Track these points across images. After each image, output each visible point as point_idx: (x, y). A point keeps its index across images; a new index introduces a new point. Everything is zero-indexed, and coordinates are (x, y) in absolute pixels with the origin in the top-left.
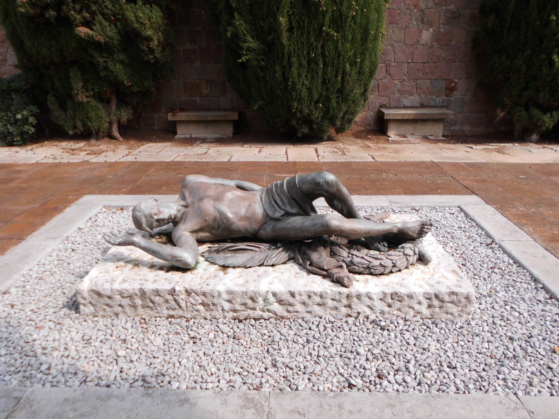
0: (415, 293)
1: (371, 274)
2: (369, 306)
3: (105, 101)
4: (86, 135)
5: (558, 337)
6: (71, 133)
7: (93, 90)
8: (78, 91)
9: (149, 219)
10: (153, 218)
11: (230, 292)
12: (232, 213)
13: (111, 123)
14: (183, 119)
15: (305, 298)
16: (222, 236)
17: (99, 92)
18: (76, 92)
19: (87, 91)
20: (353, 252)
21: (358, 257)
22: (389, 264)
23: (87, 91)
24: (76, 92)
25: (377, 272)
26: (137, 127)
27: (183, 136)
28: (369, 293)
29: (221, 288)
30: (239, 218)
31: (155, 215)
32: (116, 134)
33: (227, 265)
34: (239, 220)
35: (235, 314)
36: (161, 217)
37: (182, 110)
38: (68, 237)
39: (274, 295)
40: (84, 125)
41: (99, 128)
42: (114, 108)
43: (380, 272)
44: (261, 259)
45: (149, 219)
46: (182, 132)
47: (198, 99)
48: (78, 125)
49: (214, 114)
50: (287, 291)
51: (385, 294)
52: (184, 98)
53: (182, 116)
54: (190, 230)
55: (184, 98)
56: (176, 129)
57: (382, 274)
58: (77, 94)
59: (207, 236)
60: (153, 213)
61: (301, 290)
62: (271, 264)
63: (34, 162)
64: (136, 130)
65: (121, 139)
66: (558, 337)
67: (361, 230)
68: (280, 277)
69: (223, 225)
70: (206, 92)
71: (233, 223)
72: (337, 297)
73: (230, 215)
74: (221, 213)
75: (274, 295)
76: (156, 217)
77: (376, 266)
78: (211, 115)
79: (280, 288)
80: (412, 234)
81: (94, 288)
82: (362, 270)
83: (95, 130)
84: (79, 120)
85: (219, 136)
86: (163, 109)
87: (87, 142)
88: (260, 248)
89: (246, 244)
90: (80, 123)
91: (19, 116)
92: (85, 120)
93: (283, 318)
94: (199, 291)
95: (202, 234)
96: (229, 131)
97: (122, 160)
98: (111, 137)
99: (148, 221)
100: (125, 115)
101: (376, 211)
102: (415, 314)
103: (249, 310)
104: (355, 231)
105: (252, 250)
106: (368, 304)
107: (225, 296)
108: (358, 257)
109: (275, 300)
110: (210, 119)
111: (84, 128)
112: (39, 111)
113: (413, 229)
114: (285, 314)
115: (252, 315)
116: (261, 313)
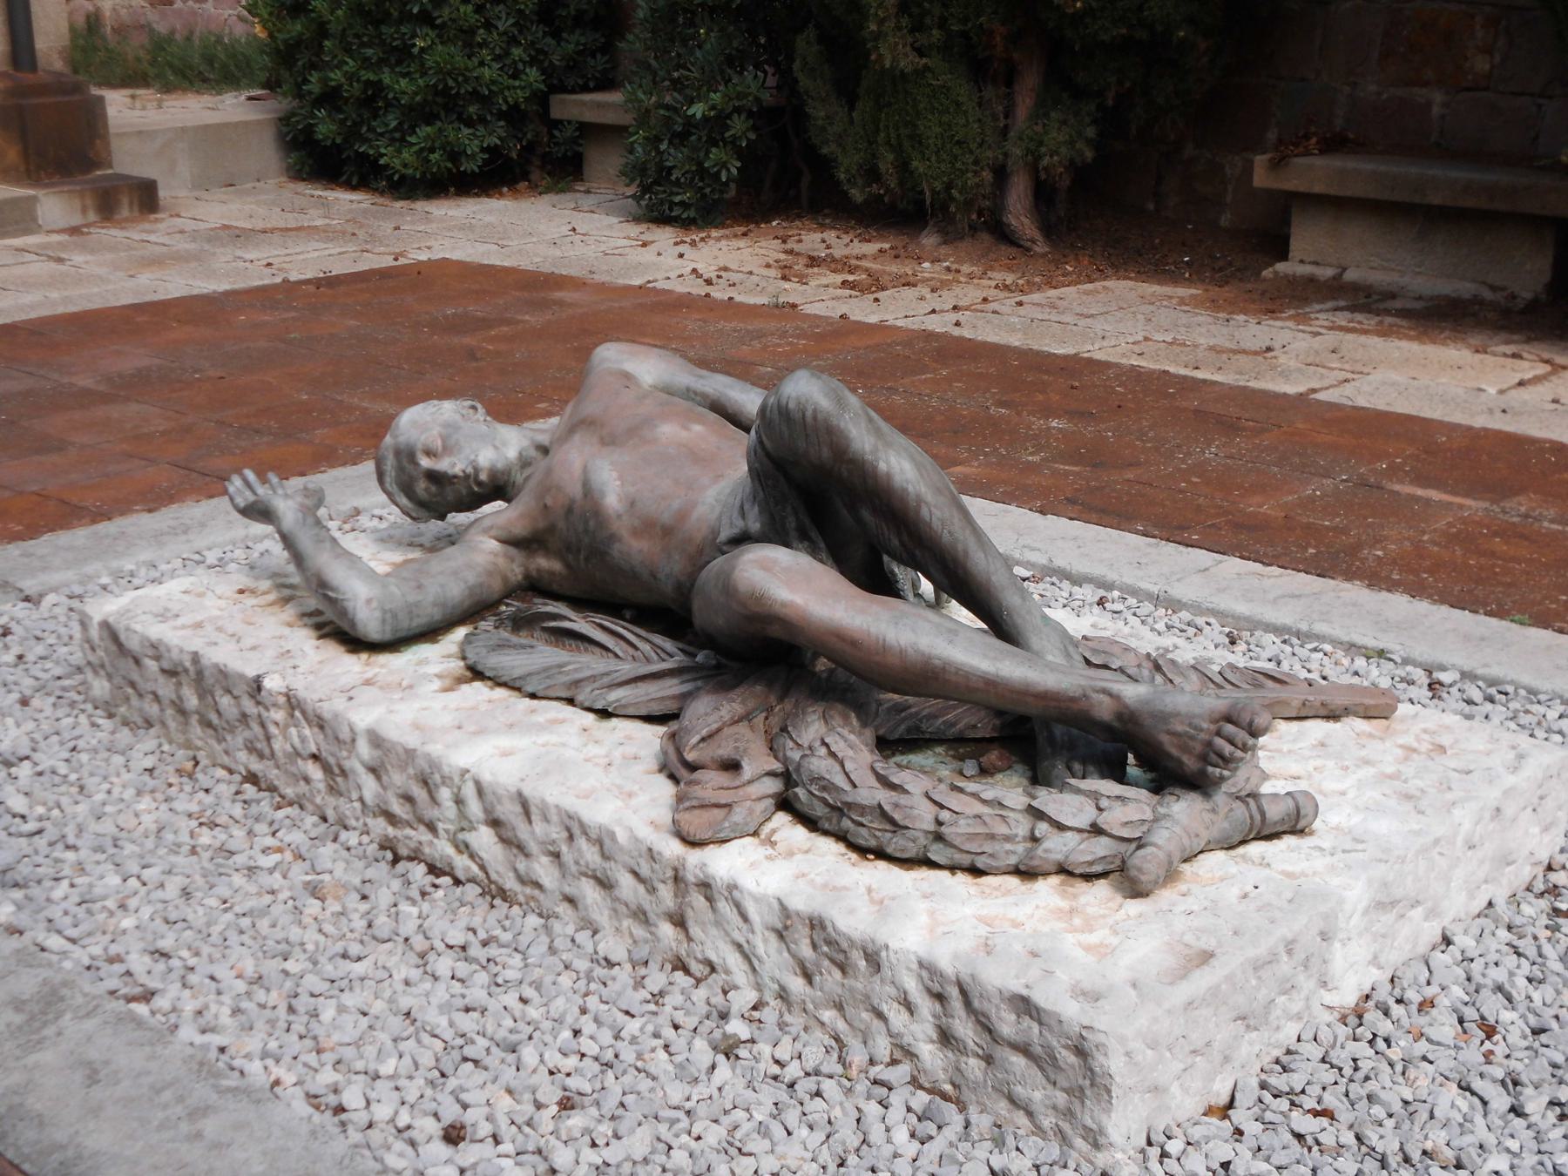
0: (887, 947)
1: (841, 837)
3: (987, 70)
4: (902, 212)
6: (857, 195)
7: (942, 24)
8: (881, 22)
10: (417, 464)
11: (376, 740)
13: (1001, 174)
14: (1318, 188)
15: (557, 833)
17: (964, 35)
18: (873, 27)
19: (918, 27)
20: (1047, 799)
22: (923, 816)
23: (918, 27)
24: (873, 27)
25: (864, 838)
26: (1151, 206)
27: (1307, 269)
30: (636, 523)
31: (429, 453)
32: (1019, 213)
33: (480, 668)
34: (635, 533)
35: (391, 831)
37: (1334, 144)
38: (357, 512)
40: (903, 167)
41: (949, 186)
42: (1024, 105)
43: (873, 843)
45: (405, 464)
46: (1312, 250)
47: (1438, 97)
48: (882, 167)
49: (1460, 174)
50: (513, 790)
52: (1373, 88)
53: (1314, 172)
54: (504, 535)
55: (1373, 88)
56: (1289, 225)
57: (881, 854)
58: (877, 36)
59: (552, 573)
60: (419, 446)
61: (550, 800)
62: (599, 706)
63: (637, 282)
64: (1104, 214)
65: (1041, 248)
67: (885, 649)
68: (577, 759)
69: (586, 540)
70: (1482, 64)
71: (613, 538)
74: (587, 489)
76: (425, 462)
78: (1443, 181)
80: (1174, 751)
81: (111, 620)
82: (819, 811)
83: (933, 191)
84: (888, 143)
85: (1463, 288)
86: (1272, 136)
87: (900, 241)
90: (891, 157)
91: (698, 110)
92: (906, 144)
93: (503, 894)
94: (309, 709)
95: (545, 563)
96: (1527, 272)
97: (900, 323)
98: (1003, 235)
100: (1065, 141)
101: (1100, 599)
102: (898, 1055)
103: (422, 828)
104: (854, 643)
107: (364, 749)
110: (1436, 199)
111: (901, 184)
113: (1180, 728)
114: (510, 883)
115: (427, 850)
116: (450, 850)
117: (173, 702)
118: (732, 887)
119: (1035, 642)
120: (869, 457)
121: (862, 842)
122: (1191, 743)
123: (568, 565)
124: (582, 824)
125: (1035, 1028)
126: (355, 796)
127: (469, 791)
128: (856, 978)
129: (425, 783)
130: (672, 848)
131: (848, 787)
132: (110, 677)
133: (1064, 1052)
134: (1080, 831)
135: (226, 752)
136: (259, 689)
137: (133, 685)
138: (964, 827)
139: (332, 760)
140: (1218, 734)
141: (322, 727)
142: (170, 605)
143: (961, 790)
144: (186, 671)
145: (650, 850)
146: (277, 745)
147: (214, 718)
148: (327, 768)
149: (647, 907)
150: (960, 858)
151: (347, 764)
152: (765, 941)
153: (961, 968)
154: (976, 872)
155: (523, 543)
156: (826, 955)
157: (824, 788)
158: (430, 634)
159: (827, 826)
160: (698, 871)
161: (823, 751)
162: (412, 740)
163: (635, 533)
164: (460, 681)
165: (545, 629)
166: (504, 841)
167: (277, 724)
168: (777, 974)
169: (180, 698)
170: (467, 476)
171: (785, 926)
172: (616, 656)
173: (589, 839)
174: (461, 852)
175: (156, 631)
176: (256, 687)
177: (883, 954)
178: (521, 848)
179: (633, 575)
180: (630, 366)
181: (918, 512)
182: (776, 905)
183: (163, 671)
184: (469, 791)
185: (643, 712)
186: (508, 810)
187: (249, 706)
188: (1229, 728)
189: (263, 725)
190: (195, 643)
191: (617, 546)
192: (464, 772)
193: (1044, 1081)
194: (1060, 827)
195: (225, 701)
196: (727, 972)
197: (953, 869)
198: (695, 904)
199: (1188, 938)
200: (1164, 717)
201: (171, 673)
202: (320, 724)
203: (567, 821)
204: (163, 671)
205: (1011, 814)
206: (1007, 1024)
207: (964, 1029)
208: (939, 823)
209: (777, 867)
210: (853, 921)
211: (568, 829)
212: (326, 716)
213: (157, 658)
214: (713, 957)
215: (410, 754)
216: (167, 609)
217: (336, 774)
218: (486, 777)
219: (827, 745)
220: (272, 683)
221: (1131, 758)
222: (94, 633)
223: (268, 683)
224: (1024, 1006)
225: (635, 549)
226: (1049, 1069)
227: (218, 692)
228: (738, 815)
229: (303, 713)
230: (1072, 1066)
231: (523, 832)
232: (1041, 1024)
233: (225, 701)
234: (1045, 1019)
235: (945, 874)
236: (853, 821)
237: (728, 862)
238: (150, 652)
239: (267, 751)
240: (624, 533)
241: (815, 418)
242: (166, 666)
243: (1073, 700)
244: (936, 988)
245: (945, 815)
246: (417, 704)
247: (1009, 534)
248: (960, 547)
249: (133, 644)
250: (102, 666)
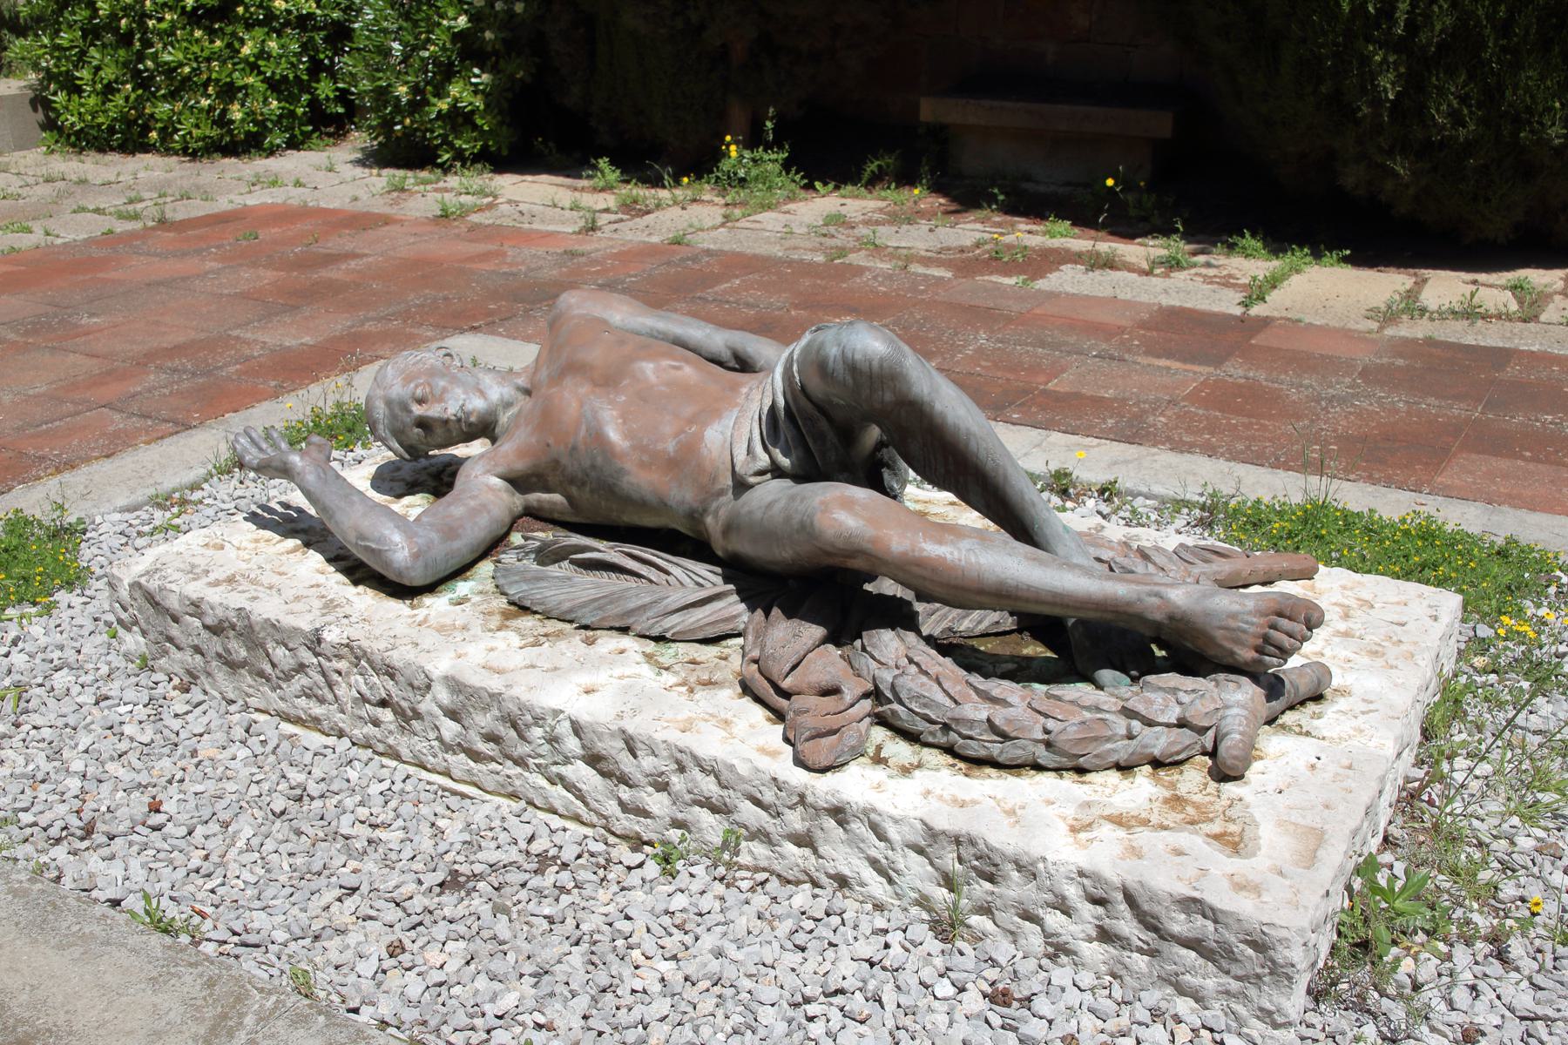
0: (1044, 859)
1: (949, 750)
2: (874, 863)
5: (3, 754)
9: (397, 410)
11: (455, 685)
12: (628, 435)
15: (665, 765)
16: (594, 514)
21: (926, 673)
25: (975, 750)
28: (874, 810)
29: (440, 666)
31: (420, 401)
33: (527, 603)
36: (433, 411)
39: (577, 729)
43: (982, 753)
44: (1365, 798)
45: (397, 410)
51: (933, 834)
59: (555, 503)
62: (655, 632)
66: (3, 754)
68: (656, 689)
72: (768, 796)
73: (614, 435)
75: (577, 729)
76: (418, 410)
77: (971, 723)
79: (598, 711)
88: (667, 573)
89: (628, 548)
94: (377, 658)
99: (394, 416)
101: (1123, 515)
103: (509, 763)
105: (639, 576)
106: (873, 853)
107: (443, 695)
108: (926, 673)
109: (579, 751)
112: (924, 160)
117: (219, 656)
118: (274, 626)
119: (1061, 550)
120: (926, 399)
121: (971, 753)
122: (1244, 636)
123: (569, 497)
124: (695, 757)
125: (1210, 926)
126: (432, 735)
127: (564, 728)
128: (1009, 887)
129: (514, 726)
130: (799, 778)
131: (948, 702)
132: (144, 633)
133: (1242, 946)
134: (1168, 725)
135: (282, 699)
136: (319, 641)
137: (170, 639)
138: (1073, 732)
139: (404, 704)
140: (1273, 627)
141: (392, 676)
142: (196, 561)
143: (1058, 698)
144: (233, 627)
145: (775, 779)
146: (342, 691)
147: (268, 668)
148: (399, 712)
149: (771, 829)
150: (1065, 761)
151: (422, 708)
152: (905, 856)
153: (1125, 876)
154: (1081, 771)
155: (518, 482)
156: (974, 868)
157: (925, 706)
158: (461, 571)
159: (931, 739)
160: (829, 797)
161: (913, 669)
162: (494, 684)
163: (642, 465)
164: (507, 616)
165: (573, 562)
166: (603, 774)
167: (339, 673)
168: (919, 884)
169: (228, 651)
170: (459, 420)
171: (929, 841)
172: (651, 581)
173: (703, 770)
174: (553, 784)
175: (194, 590)
176: (315, 642)
177: (1041, 866)
178: (624, 780)
179: (643, 505)
180: (606, 315)
181: (967, 445)
182: (919, 825)
183: (206, 627)
184: (564, 728)
185: (700, 636)
186: (612, 746)
187: (307, 657)
188: (1284, 623)
189: (324, 674)
190: (236, 600)
191: (626, 479)
192: (556, 713)
193: (1215, 970)
194: (1150, 723)
195: (280, 653)
196: (863, 885)
197: (1057, 770)
198: (825, 825)
199: (1295, 817)
200: (1207, 614)
201: (216, 630)
202: (390, 672)
203: (679, 755)
204: (206, 627)
205: (1107, 716)
206: (1178, 924)
207: (1127, 926)
208: (1047, 732)
209: (908, 791)
210: (1001, 837)
211: (678, 762)
212: (397, 664)
213: (199, 615)
214: (846, 871)
215: (496, 697)
216: (193, 566)
217: (408, 717)
218: (584, 718)
219: (918, 665)
220: (332, 636)
221: (1154, 647)
222: (124, 593)
223: (325, 635)
224: (1192, 905)
225: (641, 479)
226: (1224, 963)
227: (270, 646)
228: (850, 737)
229: (369, 662)
230: (1250, 958)
231: (626, 763)
232: (1216, 922)
233: (280, 653)
234: (1221, 917)
235: (1052, 774)
236: (960, 734)
237: (853, 784)
238: (191, 609)
239: (330, 697)
240: (628, 466)
241: (881, 367)
242: (209, 621)
243: (1128, 604)
244: (1100, 893)
245: (1050, 724)
246: (458, 640)
247: (1024, 451)
248: (1001, 471)
249: (173, 603)
250: (136, 623)
